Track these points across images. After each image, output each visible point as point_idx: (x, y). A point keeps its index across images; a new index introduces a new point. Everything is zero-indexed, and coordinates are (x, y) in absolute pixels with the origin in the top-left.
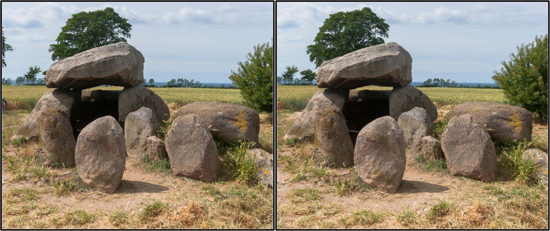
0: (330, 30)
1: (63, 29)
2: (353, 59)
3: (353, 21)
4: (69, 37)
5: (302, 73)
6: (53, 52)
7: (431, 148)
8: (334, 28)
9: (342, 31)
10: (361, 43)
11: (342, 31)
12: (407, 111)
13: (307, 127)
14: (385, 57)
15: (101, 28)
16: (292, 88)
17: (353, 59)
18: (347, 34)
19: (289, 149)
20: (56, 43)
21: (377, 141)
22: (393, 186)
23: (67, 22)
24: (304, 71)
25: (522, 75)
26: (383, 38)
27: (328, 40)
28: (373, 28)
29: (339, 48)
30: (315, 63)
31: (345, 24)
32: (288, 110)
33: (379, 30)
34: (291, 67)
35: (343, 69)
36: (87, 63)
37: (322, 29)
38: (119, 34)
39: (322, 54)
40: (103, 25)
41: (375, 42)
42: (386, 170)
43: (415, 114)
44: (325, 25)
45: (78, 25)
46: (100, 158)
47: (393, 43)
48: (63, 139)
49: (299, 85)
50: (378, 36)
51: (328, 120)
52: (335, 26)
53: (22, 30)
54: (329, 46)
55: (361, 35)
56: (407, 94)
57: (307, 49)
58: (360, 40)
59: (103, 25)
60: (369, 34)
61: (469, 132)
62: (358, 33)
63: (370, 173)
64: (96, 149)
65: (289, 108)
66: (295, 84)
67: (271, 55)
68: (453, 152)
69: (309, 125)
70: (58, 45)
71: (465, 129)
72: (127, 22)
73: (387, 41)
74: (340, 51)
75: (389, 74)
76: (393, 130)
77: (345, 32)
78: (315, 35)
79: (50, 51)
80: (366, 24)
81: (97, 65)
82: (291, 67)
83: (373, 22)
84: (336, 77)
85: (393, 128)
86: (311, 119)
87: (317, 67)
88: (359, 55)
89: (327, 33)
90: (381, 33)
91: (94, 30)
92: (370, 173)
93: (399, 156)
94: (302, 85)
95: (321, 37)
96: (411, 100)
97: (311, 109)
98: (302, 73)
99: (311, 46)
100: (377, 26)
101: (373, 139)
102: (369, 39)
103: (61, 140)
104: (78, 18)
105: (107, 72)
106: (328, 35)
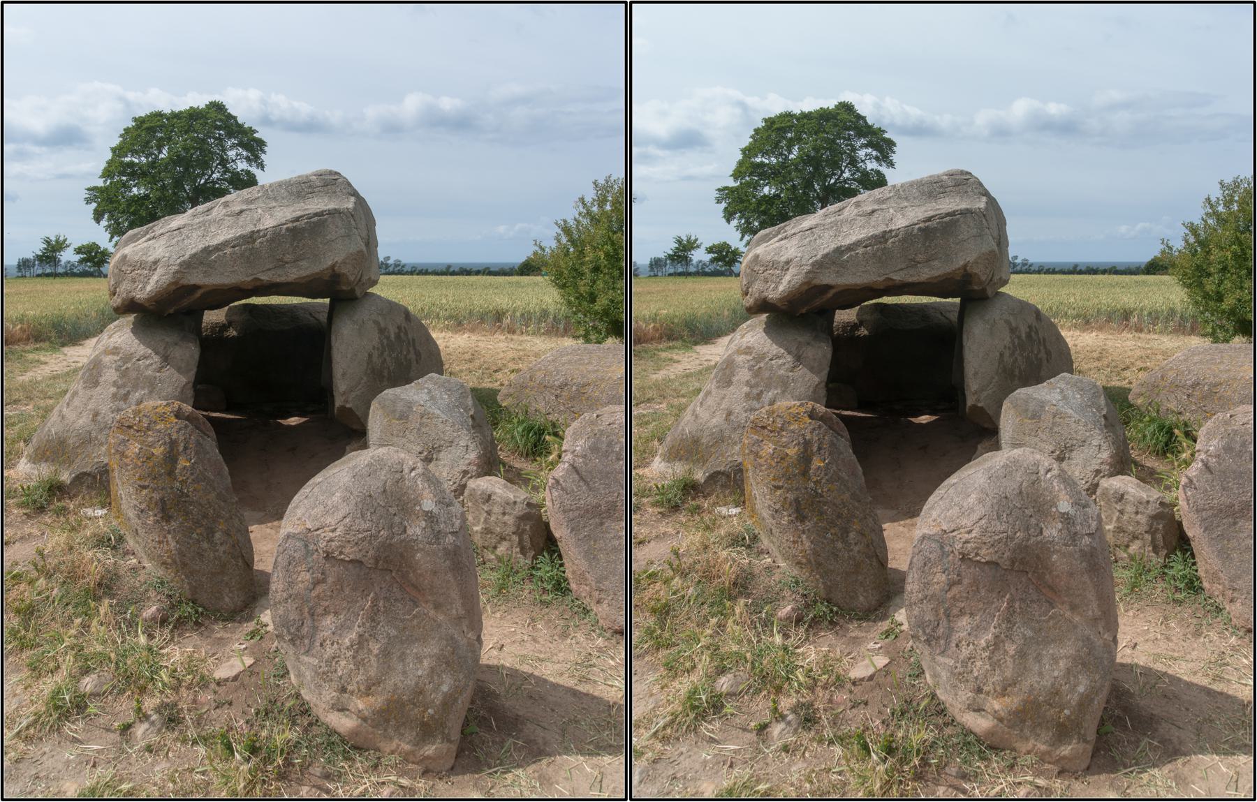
0: (134, 153)
1: (114, 150)
2: (851, 222)
3: (186, 132)
4: (759, 169)
5: (79, 251)
6: (94, 205)
7: (509, 519)
8: (144, 148)
9: (162, 156)
10: (206, 183)
11: (162, 156)
12: (1038, 380)
13: (87, 440)
14: (320, 214)
15: (830, 149)
16: (690, 283)
17: (851, 222)
18: (803, 161)
19: (27, 530)
20: (100, 183)
21: (1005, 564)
22: (445, 746)
23: (121, 136)
24: (83, 247)
25: (607, 254)
26: (254, 170)
27: (133, 175)
28: (233, 146)
29: (158, 193)
30: (737, 228)
31: (799, 140)
32: (46, 345)
33: (245, 153)
34: (53, 239)
35: (826, 256)
36: (874, 237)
37: (748, 152)
38: (238, 162)
39: (752, 207)
40: (204, 141)
41: (248, 181)
42: (1047, 683)
43: (432, 398)
44: (124, 142)
45: (148, 142)
46: (386, 630)
47: (331, 173)
48: (205, 516)
49: (74, 275)
50: (242, 166)
51: (158, 451)
52: (777, 145)
53: (660, 153)
54: (135, 190)
55: (205, 165)
56: (1008, 322)
57: (85, 194)
58: (204, 174)
59: (204, 141)
60: (224, 162)
62: (197, 160)
63: (979, 690)
64: (1001, 596)
65: (49, 338)
66: (65, 275)
67: (615, 211)
68: (600, 544)
69: (727, 434)
70: (107, 188)
72: (886, 135)
73: (264, 178)
74: (159, 199)
76: (430, 517)
77: (800, 157)
78: (734, 166)
79: (88, 201)
80: (216, 139)
81: (904, 240)
82: (53, 239)
83: (230, 135)
84: (803, 284)
85: (428, 504)
86: (96, 414)
87: (112, 237)
88: (237, 209)
89: (128, 159)
90: (248, 159)
91: (813, 153)
92: (979, 690)
93: (1095, 620)
94: (84, 274)
95: (747, 168)
96: (388, 338)
97: (96, 384)
98: (79, 251)
99: (726, 188)
100: (241, 144)
101: (350, 553)
102: (225, 173)
103: (198, 523)
104: (145, 126)
105: (304, 263)
106: (762, 165)
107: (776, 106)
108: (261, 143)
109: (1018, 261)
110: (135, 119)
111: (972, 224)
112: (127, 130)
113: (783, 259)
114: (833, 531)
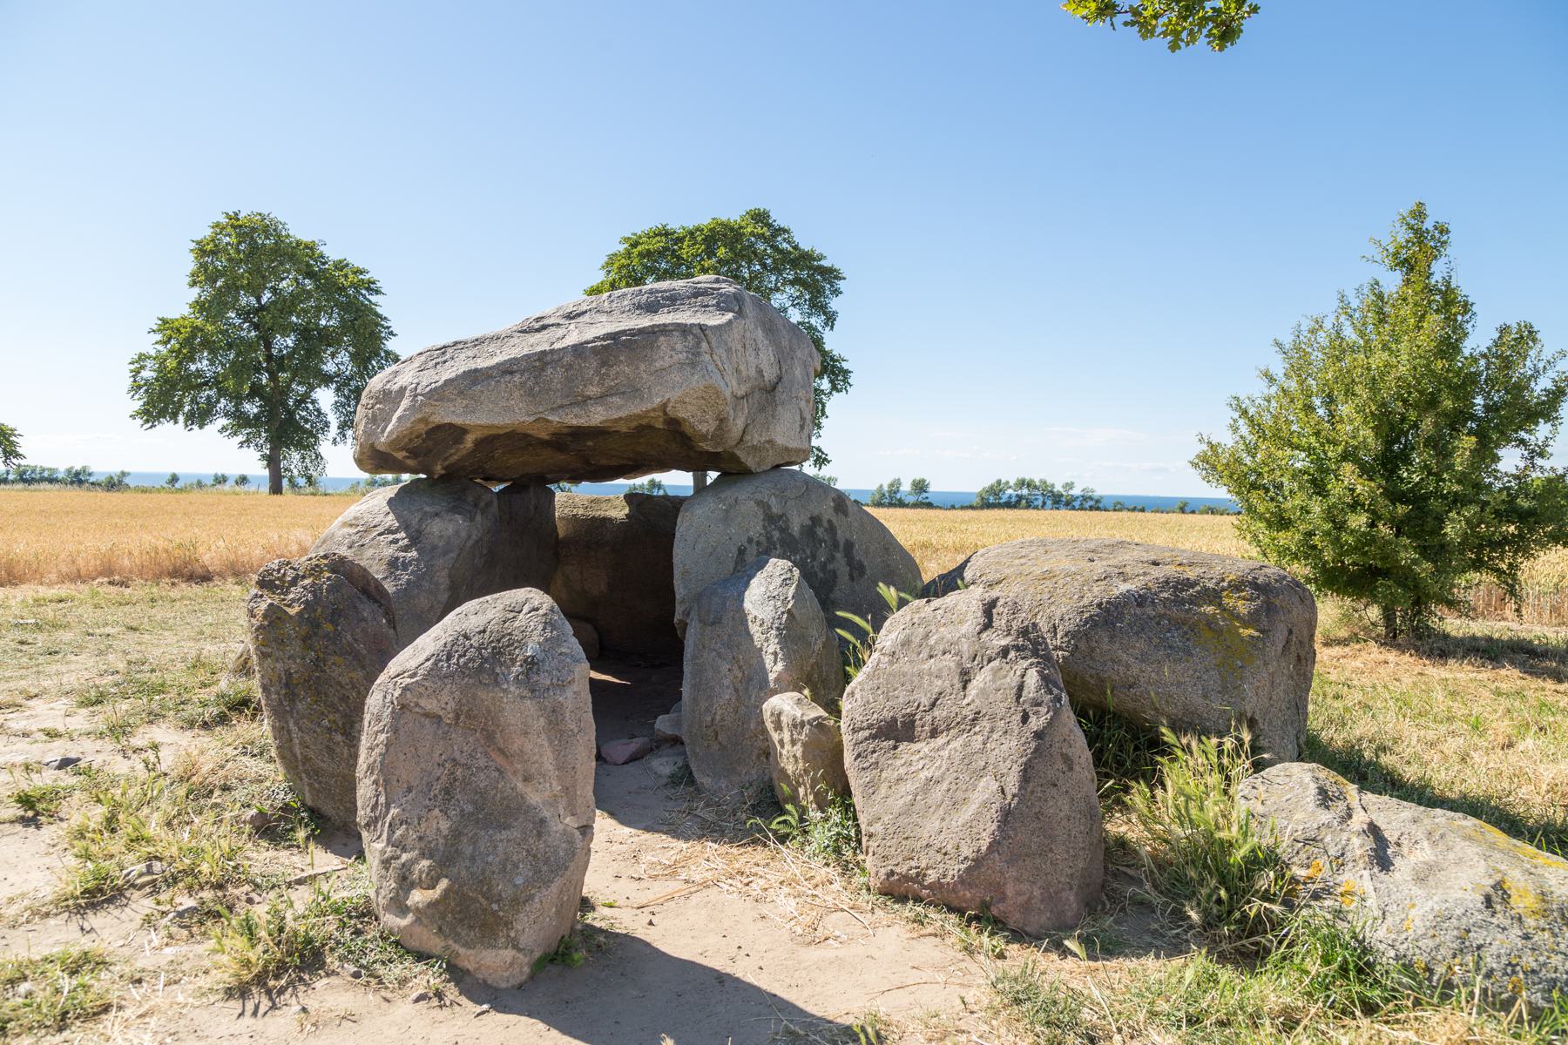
61: (965, 678)
71: (949, 662)
75: (664, 406)
107: (642, 223)
108: (831, 274)
109: (1076, 492)
110: (626, 239)
111: (679, 347)
112: (612, 258)
113: (396, 387)
114: (331, 717)
